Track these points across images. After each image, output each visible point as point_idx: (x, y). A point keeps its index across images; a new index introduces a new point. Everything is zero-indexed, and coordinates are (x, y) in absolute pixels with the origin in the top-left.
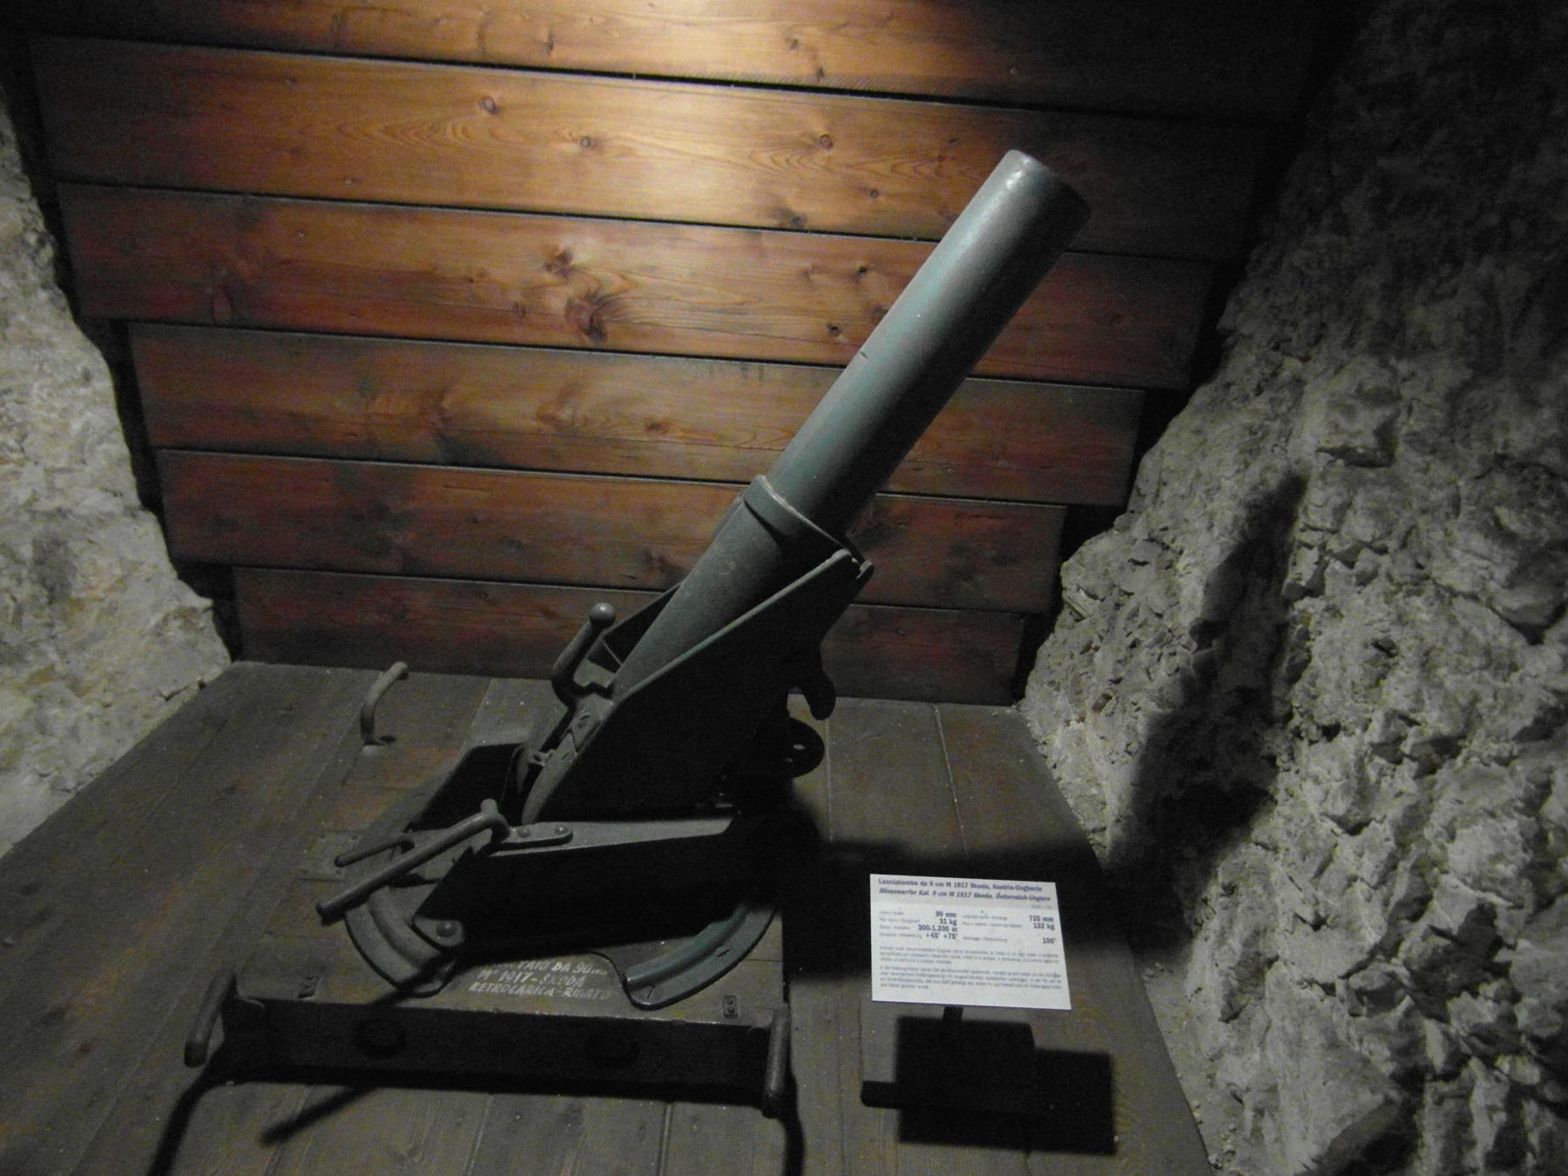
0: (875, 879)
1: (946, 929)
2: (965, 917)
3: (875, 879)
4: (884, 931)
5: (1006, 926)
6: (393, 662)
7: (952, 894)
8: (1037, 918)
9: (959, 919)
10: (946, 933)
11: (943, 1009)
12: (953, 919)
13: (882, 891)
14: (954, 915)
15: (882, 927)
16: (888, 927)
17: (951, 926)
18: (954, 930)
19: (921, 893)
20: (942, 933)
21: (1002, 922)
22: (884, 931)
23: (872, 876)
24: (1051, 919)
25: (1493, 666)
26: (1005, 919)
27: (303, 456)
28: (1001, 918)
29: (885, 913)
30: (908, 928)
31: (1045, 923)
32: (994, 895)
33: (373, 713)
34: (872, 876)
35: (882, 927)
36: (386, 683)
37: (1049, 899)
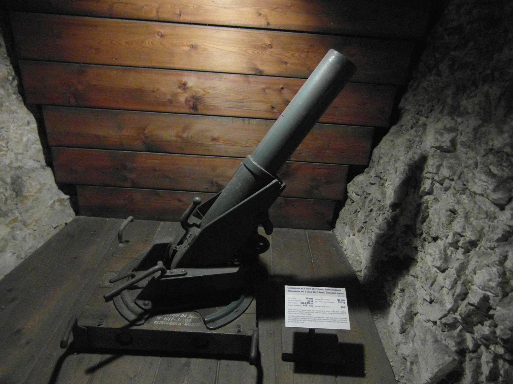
0: (286, 287)
1: (309, 303)
2: (316, 299)
3: (286, 287)
4: (289, 304)
5: (329, 302)
6: (129, 216)
7: (311, 292)
8: (339, 300)
9: (314, 300)
10: (309, 305)
11: (308, 329)
12: (312, 300)
13: (289, 291)
14: (312, 299)
15: (288, 303)
16: (290, 303)
17: (311, 302)
18: (312, 304)
19: (301, 292)
20: (308, 305)
21: (328, 301)
22: (289, 304)
23: (285, 286)
24: (344, 300)
25: (488, 218)
26: (329, 300)
27: (99, 149)
28: (327, 300)
29: (289, 298)
30: (297, 303)
31: (342, 301)
32: (325, 292)
33: (122, 233)
34: (285, 286)
35: (288, 303)
36: (126, 223)
37: (343, 294)
